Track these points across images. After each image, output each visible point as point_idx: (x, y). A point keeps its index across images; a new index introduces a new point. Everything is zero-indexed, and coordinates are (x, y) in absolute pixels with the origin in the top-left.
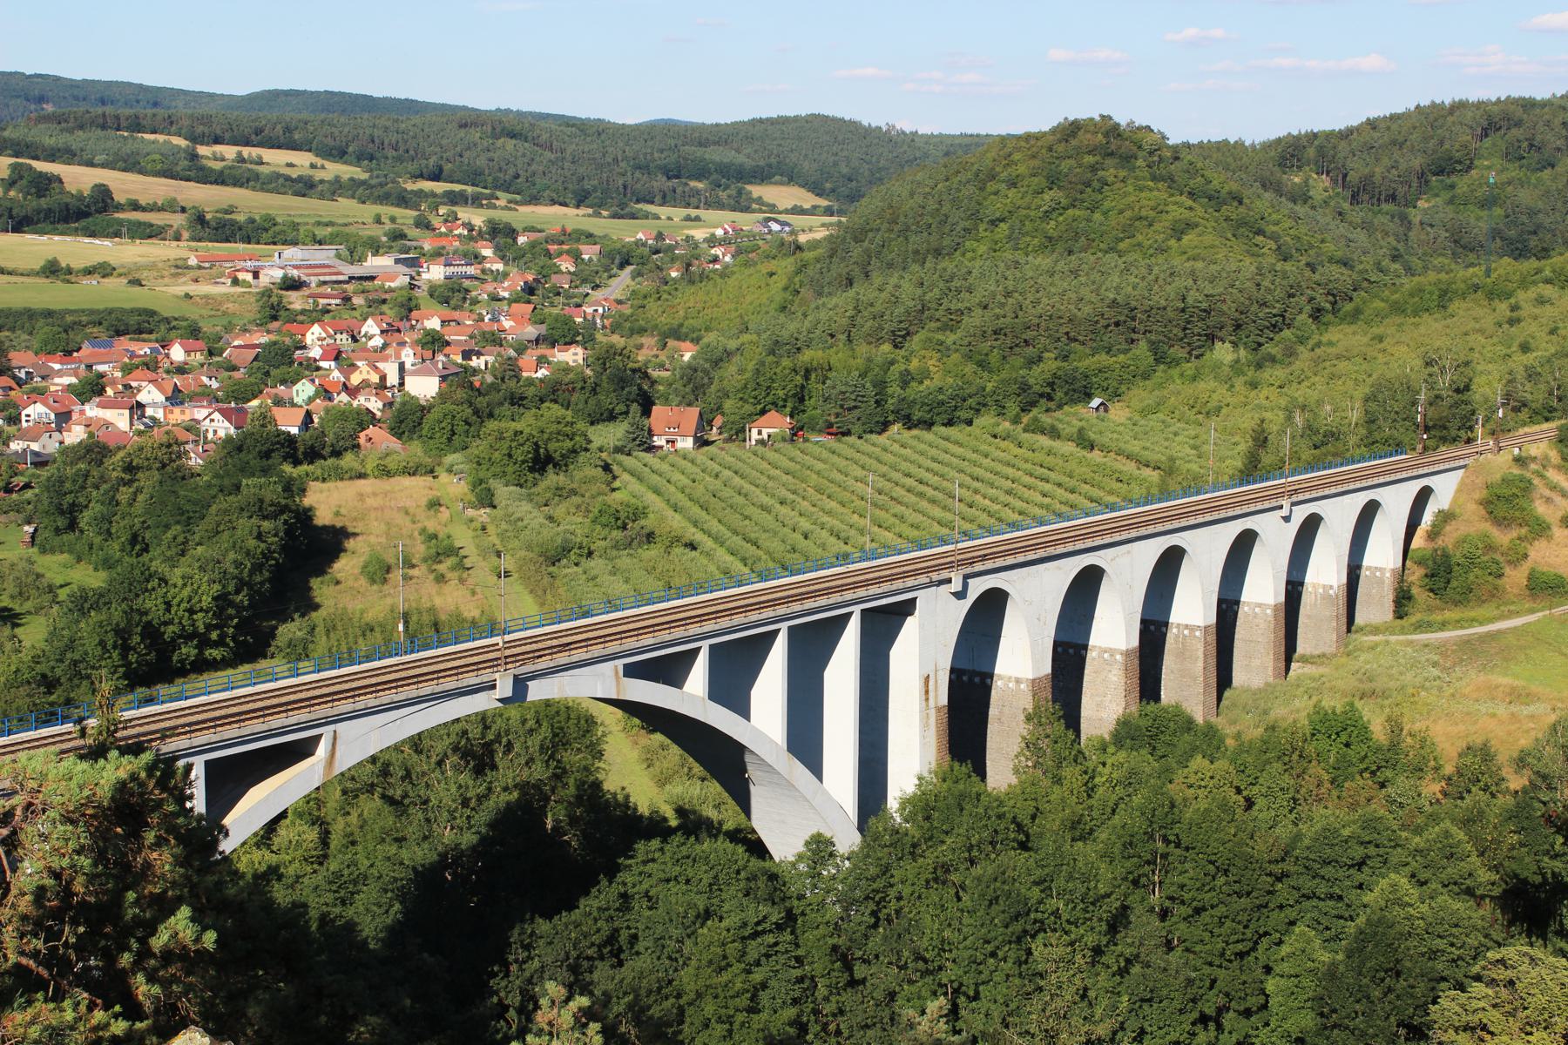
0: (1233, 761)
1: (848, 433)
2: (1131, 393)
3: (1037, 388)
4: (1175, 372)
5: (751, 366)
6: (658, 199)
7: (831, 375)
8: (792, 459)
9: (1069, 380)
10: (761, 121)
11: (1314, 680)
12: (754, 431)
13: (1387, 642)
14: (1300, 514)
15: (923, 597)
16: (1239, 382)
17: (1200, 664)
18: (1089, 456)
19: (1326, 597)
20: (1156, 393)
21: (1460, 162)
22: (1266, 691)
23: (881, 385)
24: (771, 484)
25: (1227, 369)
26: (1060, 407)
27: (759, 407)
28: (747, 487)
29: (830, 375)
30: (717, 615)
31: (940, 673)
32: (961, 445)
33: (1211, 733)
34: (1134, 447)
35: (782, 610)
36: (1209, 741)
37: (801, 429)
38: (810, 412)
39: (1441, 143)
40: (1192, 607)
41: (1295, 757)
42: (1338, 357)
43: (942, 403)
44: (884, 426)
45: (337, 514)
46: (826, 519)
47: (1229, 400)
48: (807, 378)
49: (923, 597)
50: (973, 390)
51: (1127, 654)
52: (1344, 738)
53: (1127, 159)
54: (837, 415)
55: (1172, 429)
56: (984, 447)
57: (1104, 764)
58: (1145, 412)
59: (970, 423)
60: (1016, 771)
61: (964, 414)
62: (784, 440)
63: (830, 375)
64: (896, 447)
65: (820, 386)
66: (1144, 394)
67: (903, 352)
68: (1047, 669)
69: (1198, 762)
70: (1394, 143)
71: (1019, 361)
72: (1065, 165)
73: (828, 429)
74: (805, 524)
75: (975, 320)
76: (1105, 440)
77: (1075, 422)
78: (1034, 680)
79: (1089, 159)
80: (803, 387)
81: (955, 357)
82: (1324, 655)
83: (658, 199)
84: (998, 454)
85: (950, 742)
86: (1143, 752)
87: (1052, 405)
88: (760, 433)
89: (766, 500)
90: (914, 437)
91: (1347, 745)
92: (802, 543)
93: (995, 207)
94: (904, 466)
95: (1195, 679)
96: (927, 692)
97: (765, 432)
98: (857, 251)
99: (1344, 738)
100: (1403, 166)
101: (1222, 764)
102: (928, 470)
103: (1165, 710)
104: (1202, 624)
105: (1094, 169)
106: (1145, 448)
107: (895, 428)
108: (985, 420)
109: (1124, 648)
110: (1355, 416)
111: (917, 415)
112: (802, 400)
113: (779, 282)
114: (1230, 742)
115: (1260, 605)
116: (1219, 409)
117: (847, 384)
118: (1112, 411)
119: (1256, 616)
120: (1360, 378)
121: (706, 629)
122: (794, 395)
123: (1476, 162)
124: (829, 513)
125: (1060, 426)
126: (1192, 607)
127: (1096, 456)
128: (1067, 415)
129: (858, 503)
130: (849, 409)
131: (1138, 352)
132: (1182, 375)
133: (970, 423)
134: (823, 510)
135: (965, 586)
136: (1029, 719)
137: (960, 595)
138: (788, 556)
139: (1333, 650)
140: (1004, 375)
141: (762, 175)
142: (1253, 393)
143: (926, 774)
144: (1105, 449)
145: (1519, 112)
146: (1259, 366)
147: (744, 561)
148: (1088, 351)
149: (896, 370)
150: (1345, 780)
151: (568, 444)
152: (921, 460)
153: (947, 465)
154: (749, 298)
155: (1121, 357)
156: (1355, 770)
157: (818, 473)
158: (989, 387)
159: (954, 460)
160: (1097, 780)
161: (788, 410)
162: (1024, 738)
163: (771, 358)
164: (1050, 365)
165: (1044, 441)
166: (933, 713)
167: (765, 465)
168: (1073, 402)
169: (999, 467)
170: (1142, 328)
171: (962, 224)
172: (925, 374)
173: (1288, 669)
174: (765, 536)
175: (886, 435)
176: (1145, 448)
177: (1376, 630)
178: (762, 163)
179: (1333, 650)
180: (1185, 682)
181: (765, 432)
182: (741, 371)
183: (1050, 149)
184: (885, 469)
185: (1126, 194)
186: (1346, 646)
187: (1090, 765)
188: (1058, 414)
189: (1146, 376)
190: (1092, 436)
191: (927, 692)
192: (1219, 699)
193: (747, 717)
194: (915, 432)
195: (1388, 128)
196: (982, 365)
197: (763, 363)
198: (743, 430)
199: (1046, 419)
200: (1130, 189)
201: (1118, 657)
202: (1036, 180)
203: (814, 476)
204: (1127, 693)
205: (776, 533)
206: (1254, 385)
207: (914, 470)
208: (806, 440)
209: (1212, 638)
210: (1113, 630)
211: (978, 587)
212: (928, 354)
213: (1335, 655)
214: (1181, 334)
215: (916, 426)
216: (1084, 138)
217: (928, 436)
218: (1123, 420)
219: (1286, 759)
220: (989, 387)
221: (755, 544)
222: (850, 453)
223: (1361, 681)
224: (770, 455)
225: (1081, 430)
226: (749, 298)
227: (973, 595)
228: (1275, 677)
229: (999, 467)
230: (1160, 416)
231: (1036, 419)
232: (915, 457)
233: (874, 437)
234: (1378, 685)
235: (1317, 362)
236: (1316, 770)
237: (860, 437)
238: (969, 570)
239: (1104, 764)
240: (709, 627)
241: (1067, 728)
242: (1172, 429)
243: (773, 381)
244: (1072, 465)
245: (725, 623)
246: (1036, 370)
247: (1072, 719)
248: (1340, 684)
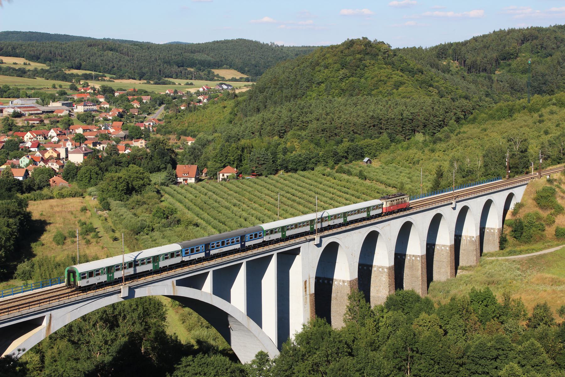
6: (174, 76)
10: (217, 42)
21: (512, 55)
39: (505, 46)
72: (348, 59)
75: (314, 125)
79: (358, 56)
83: (174, 76)
88: (223, 175)
93: (319, 77)
97: (226, 175)
98: (261, 97)
100: (489, 57)
105: (360, 60)
113: (228, 110)
123: (519, 55)
141: (219, 65)
145: (536, 33)
151: (141, 182)
154: (215, 118)
171: (305, 85)
178: (218, 60)
185: (374, 71)
195: (482, 41)
200: (376, 68)
202: (336, 65)
214: (401, 130)
216: (356, 47)
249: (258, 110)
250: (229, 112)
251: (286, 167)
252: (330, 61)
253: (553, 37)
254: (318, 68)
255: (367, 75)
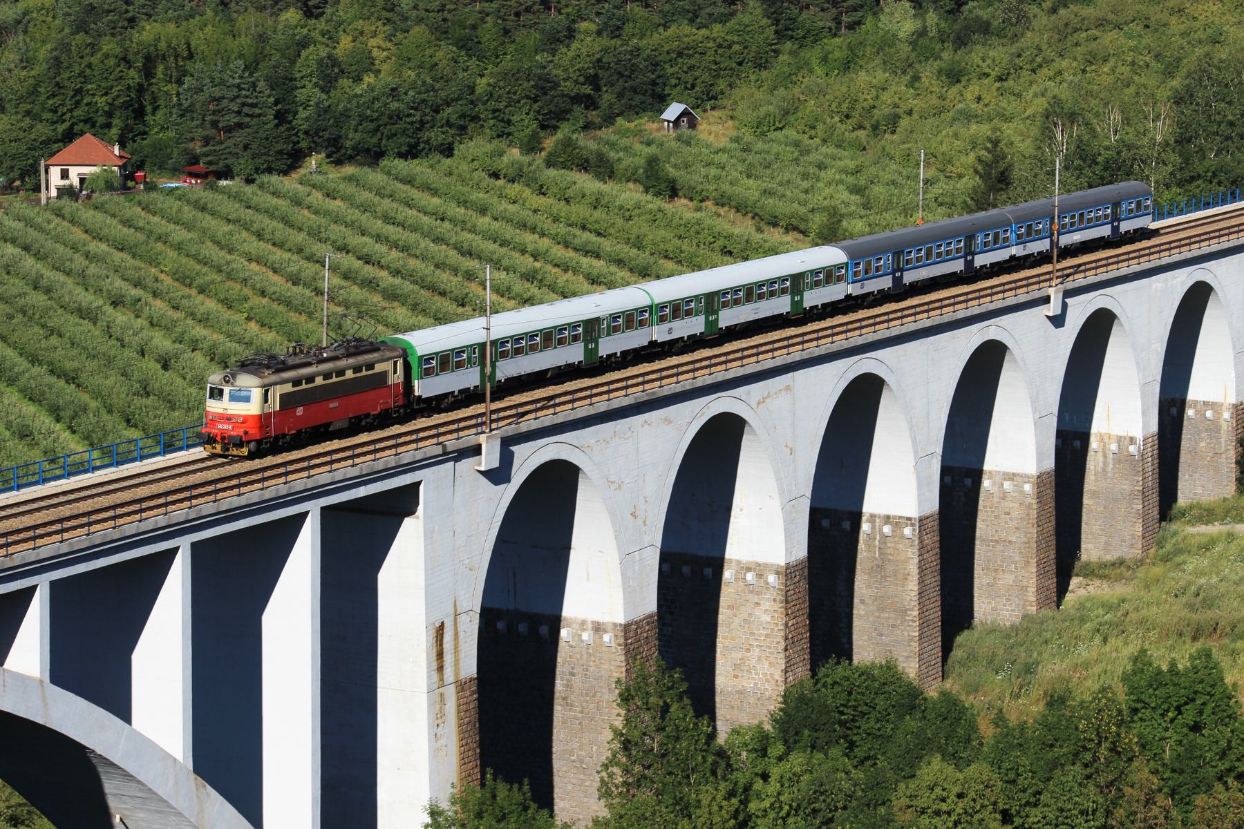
0: (996, 764)
1: (227, 174)
2: (737, 93)
3: (567, 87)
4: (812, 54)
5: (43, 53)
7: (196, 66)
8: (127, 223)
9: (626, 71)
11: (1109, 607)
12: (55, 172)
13: (1231, 537)
14: (1080, 310)
15: (431, 483)
16: (928, 73)
17: (913, 586)
18: (668, 207)
19: (1122, 458)
20: (781, 91)
22: (1026, 630)
23: (284, 85)
24: (92, 269)
25: (906, 48)
26: (609, 120)
27: (61, 128)
28: (50, 275)
29: (189, 66)
30: (62, 525)
31: (463, 619)
32: (435, 192)
33: (952, 714)
34: (749, 189)
35: (179, 513)
36: (950, 728)
37: (140, 166)
38: (156, 135)
40: (899, 485)
41: (1103, 752)
42: (1101, 23)
43: (397, 116)
44: (294, 159)
45: (775, 600)
46: (199, 331)
47: (912, 103)
48: (148, 72)
49: (431, 483)
50: (454, 89)
51: (788, 572)
52: (1189, 715)
54: (207, 141)
55: (814, 157)
56: (477, 196)
57: (765, 777)
58: (762, 127)
59: (448, 151)
60: (605, 792)
61: (435, 136)
62: (109, 187)
63: (189, 66)
64: (317, 197)
65: (172, 88)
66: (759, 95)
67: (321, 24)
68: (650, 604)
69: (934, 768)
71: (530, 38)
73: (191, 167)
74: (162, 342)
76: (695, 177)
77: (638, 147)
78: (626, 627)
80: (141, 89)
81: (419, 32)
82: (1121, 562)
84: (504, 206)
85: (482, 744)
86: (835, 752)
87: (594, 116)
88: (65, 175)
89: (86, 298)
90: (350, 179)
91: (1196, 728)
92: (164, 379)
94: (336, 231)
95: (904, 612)
96: (440, 655)
99: (1189, 715)
101: (979, 770)
102: (378, 238)
103: (866, 673)
104: (914, 513)
106: (767, 193)
107: (313, 162)
108: (477, 146)
109: (781, 561)
110: (1161, 131)
111: (352, 138)
112: (140, 114)
114: (987, 730)
115: (1011, 477)
116: (894, 120)
117: (223, 82)
118: (703, 126)
119: (1004, 496)
120: (1141, 60)
121: (44, 553)
122: (126, 105)
124: (205, 320)
125: (613, 155)
126: (899, 485)
127: (682, 208)
128: (624, 133)
129: (256, 300)
130: (229, 130)
131: (746, 19)
132: (825, 60)
133: (448, 151)
134: (192, 315)
135: (507, 459)
136: (626, 698)
137: (498, 475)
138: (138, 402)
139: (1137, 552)
140: (507, 63)
142: (954, 90)
143: (445, 805)
144: (697, 196)
146: (961, 42)
147: (56, 412)
148: (656, 18)
149: (311, 55)
150: (1195, 790)
152: (365, 219)
153: (415, 229)
155: (717, 28)
156: (1212, 772)
157: (179, 247)
158: (482, 84)
159: (426, 220)
160: (753, 806)
161: (115, 132)
162: (618, 734)
163: (81, 38)
164: (589, 42)
165: (586, 182)
166: (451, 692)
167: (78, 235)
168: (634, 110)
169: (509, 232)
172: (367, 64)
173: (1062, 589)
174: (91, 365)
175: (295, 176)
176: (767, 193)
177: (1207, 514)
179: (1137, 552)
180: (889, 623)
181: (74, 172)
182: (27, 62)
184: (300, 237)
186: (1160, 545)
187: (742, 778)
188: (607, 133)
189: (761, 64)
190: (672, 172)
191: (440, 655)
192: (947, 648)
193: (124, 712)
194: (349, 170)
196: (468, 45)
197: (65, 47)
198: (33, 170)
199: (587, 143)
201: (772, 579)
203: (172, 254)
204: (790, 642)
205: (110, 361)
206: (954, 76)
207: (355, 240)
208: (151, 187)
209: (932, 540)
210: (764, 530)
211: (529, 458)
212: (368, 27)
213: (1141, 562)
215: (350, 159)
217: (375, 177)
218: (723, 142)
219: (1088, 756)
220: (482, 84)
221: (72, 378)
222: (233, 209)
223: (1191, 607)
224: (88, 215)
225: (652, 162)
227: (519, 475)
228: (1041, 604)
229: (509, 232)
230: (791, 133)
231: (568, 144)
232: (353, 214)
233: (275, 179)
234: (1222, 614)
235: (1065, 32)
236: (1141, 773)
237: (249, 181)
238: (511, 430)
239: (765, 777)
240: (49, 547)
241: (698, 715)
242: (814, 157)
243: (86, 80)
244: (639, 226)
245: (78, 539)
246: (566, 54)
247: (703, 698)
248: (1152, 613)
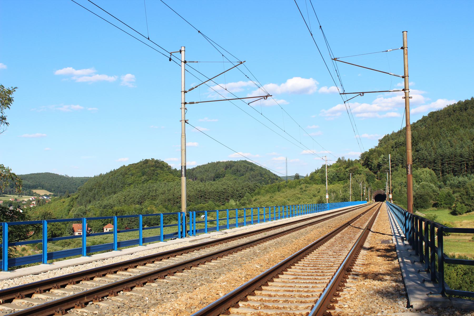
6: (8, 193)
10: (33, 174)
39: (217, 171)
53: (161, 168)
70: (206, 171)
72: (147, 170)
75: (162, 197)
79: (152, 168)
83: (8, 193)
88: (107, 230)
93: (129, 181)
97: (108, 229)
98: (91, 194)
105: (154, 170)
113: (66, 204)
141: (36, 188)
145: (233, 164)
151: (60, 232)
154: (58, 209)
170: (208, 197)
171: (121, 185)
178: (35, 184)
183: (141, 166)
185: (164, 176)
200: (165, 175)
202: (139, 174)
216: (150, 163)
226: (58, 209)
249: (90, 202)
250: (67, 204)
251: (150, 223)
252: (134, 172)
253: (242, 165)
254: (126, 176)
255: (159, 179)
